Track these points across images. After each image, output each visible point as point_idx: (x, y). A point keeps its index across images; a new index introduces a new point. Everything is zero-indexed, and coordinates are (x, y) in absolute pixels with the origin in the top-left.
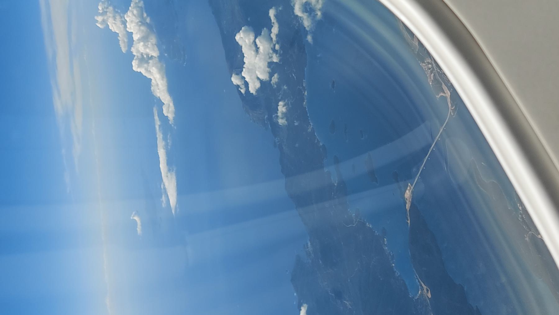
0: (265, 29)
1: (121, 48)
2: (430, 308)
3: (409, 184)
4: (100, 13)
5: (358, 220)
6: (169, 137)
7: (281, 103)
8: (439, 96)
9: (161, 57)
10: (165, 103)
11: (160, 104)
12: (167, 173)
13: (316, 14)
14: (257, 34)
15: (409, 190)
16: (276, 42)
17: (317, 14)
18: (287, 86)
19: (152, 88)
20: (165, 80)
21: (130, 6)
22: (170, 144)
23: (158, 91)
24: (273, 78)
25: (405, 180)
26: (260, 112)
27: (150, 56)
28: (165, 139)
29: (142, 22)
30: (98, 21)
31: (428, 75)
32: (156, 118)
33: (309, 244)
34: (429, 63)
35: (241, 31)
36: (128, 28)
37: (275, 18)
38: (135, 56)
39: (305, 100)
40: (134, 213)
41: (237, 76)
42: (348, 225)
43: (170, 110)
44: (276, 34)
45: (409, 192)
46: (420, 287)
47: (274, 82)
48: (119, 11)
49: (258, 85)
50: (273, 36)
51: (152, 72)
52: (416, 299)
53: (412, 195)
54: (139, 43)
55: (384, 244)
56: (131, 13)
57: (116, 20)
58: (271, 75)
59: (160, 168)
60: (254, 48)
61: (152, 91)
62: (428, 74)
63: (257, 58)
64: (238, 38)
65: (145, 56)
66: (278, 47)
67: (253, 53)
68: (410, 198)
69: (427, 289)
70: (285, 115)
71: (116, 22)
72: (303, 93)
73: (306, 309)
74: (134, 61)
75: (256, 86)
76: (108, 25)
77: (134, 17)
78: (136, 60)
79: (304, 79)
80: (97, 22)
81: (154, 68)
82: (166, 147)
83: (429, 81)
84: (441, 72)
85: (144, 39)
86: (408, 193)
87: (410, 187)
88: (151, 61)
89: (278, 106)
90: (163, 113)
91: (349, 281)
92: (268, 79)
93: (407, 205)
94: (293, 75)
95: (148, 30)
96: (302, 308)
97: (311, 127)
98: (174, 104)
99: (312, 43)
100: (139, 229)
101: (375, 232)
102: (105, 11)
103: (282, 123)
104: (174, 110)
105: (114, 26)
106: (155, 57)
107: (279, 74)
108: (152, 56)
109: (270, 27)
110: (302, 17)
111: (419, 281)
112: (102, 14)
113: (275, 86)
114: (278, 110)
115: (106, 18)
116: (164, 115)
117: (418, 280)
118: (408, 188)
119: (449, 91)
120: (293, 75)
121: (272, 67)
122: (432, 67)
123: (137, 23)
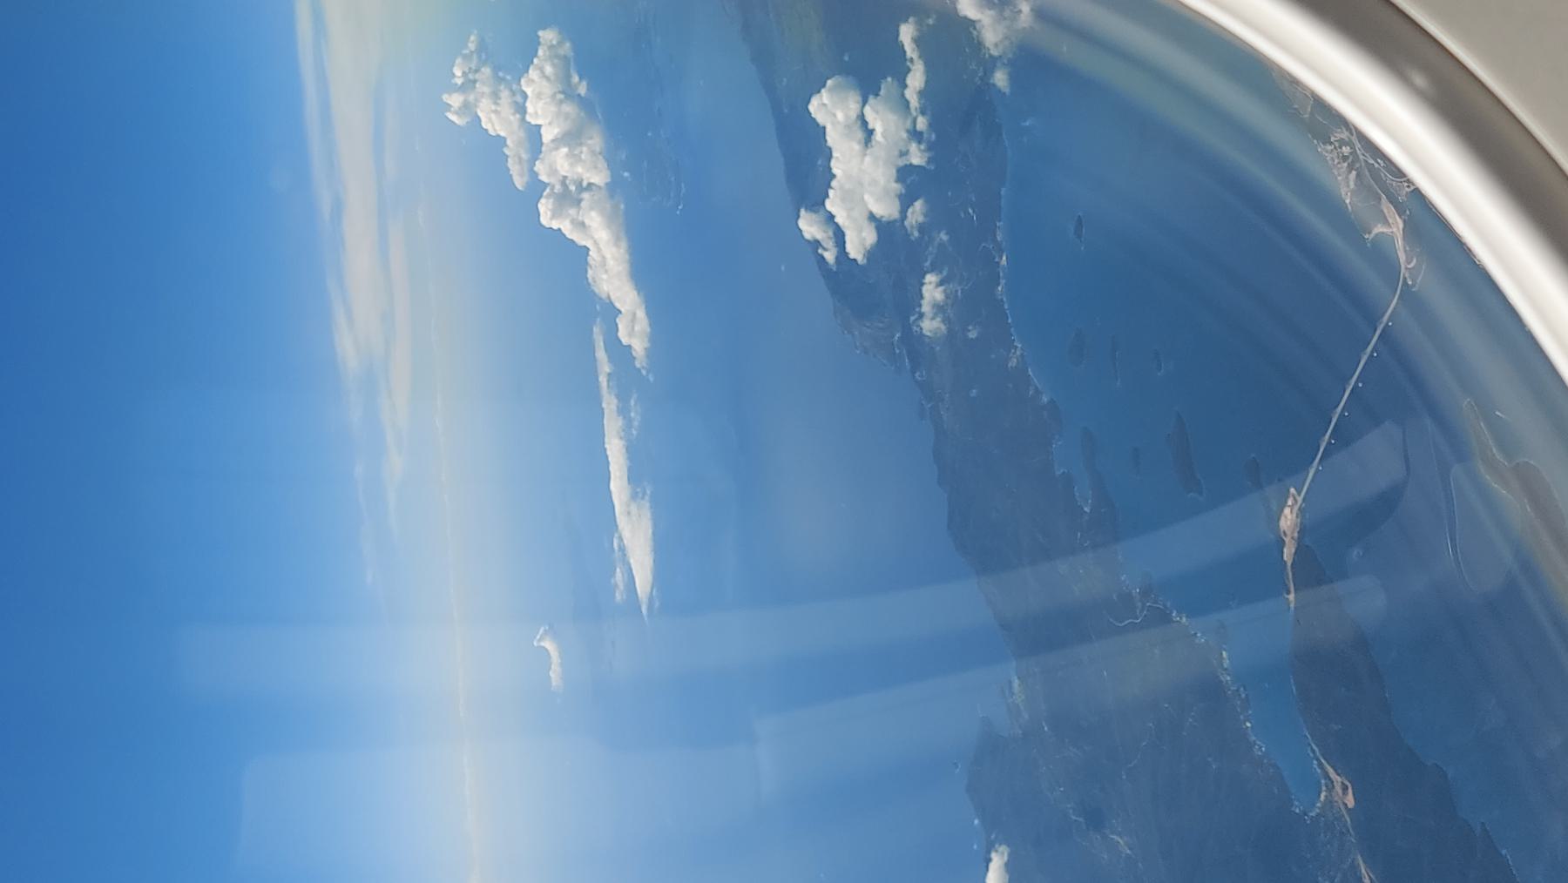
0: (889, 79)
1: (511, 176)
2: (1353, 840)
4: (456, 84)
5: (1148, 604)
6: (632, 403)
7: (931, 278)
9: (613, 187)
10: (623, 310)
11: (611, 312)
12: (628, 506)
13: (1016, 10)
14: (868, 90)
15: (1292, 507)
16: (918, 110)
17: (1020, 11)
18: (947, 234)
19: (590, 272)
20: (624, 244)
21: (535, 55)
22: (636, 424)
23: (605, 277)
24: (910, 210)
25: (1279, 480)
26: (881, 325)
27: (585, 184)
28: (623, 411)
29: (568, 93)
30: (450, 106)
31: (1339, 178)
32: (601, 354)
33: (1016, 683)
34: (1342, 143)
35: (823, 91)
36: (531, 115)
37: (915, 46)
38: (545, 185)
39: (1001, 280)
40: (541, 631)
41: (814, 216)
42: (1121, 622)
44: (918, 89)
45: (1291, 512)
46: (1323, 781)
47: (914, 222)
48: (508, 77)
49: (870, 236)
50: (911, 95)
51: (590, 227)
52: (1312, 817)
53: (1299, 520)
54: (557, 149)
55: (1222, 665)
56: (538, 72)
57: (499, 101)
58: (906, 201)
59: (610, 492)
60: (860, 135)
61: (590, 280)
62: (1339, 175)
63: (867, 159)
64: (814, 107)
65: (572, 188)
66: (923, 123)
67: (857, 147)
68: (1294, 530)
69: (1342, 783)
70: (939, 308)
71: (499, 109)
72: (997, 260)
73: (1006, 858)
74: (543, 201)
75: (864, 239)
76: (479, 118)
77: (545, 83)
78: (548, 197)
79: (1000, 221)
80: (450, 111)
81: (593, 214)
83: (1343, 193)
84: (1376, 165)
85: (571, 138)
86: (1289, 517)
87: (1295, 499)
88: (586, 195)
89: (923, 284)
91: (1124, 777)
92: (896, 215)
93: (1285, 550)
94: (970, 211)
95: (582, 114)
96: (993, 855)
97: (1018, 353)
98: (648, 314)
99: (1007, 91)
100: (555, 674)
101: (1197, 637)
102: (470, 81)
103: (930, 331)
104: (648, 330)
105: (496, 120)
106: (599, 187)
107: (926, 201)
108: (590, 184)
109: (901, 74)
110: (980, 21)
111: (1320, 764)
112: (462, 89)
113: (916, 234)
114: (922, 297)
115: (471, 98)
116: (620, 341)
117: (1318, 760)
118: (1290, 503)
119: (1400, 216)
120: (970, 211)
121: (908, 182)
122: (1351, 153)
123: (553, 96)
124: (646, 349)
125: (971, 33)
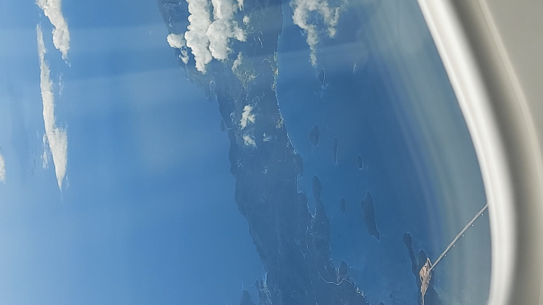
3: (428, 259)
7: (248, 108)
11: (48, 27)
15: (427, 268)
23: (47, 8)
43: (64, 38)
58: (232, 57)
90: (53, 43)
118: (426, 265)
124: (69, 42)
125: (301, 34)
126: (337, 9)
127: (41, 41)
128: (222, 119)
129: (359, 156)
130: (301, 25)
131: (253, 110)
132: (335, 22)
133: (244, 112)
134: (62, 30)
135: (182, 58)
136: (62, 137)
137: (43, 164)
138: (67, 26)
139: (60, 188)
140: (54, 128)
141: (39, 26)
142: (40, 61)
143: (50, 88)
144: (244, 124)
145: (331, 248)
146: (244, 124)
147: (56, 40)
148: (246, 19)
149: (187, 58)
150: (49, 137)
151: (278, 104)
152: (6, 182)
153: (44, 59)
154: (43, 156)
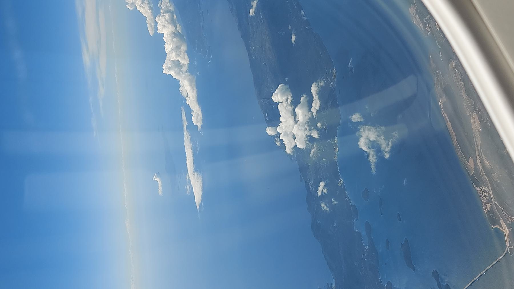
7: (322, 184)
8: (495, 227)
9: (191, 66)
11: (189, 111)
20: (195, 91)
23: (188, 99)
28: (192, 140)
43: (153, 30)
81: (185, 81)
82: (194, 149)
126: (390, 140)
127: (184, 118)
128: (300, 174)
129: (398, 213)
130: (365, 149)
131: (326, 185)
132: (389, 149)
133: (319, 186)
134: (198, 113)
135: (276, 143)
136: (199, 179)
137: (187, 192)
138: (201, 110)
139: (198, 209)
140: (194, 173)
141: (183, 108)
142: (184, 129)
143: (191, 147)
144: (319, 193)
145: (380, 271)
146: (319, 193)
147: (194, 119)
148: (319, 125)
149: (280, 142)
150: (191, 178)
151: (339, 170)
152: (162, 195)
153: (187, 128)
154: (186, 187)
